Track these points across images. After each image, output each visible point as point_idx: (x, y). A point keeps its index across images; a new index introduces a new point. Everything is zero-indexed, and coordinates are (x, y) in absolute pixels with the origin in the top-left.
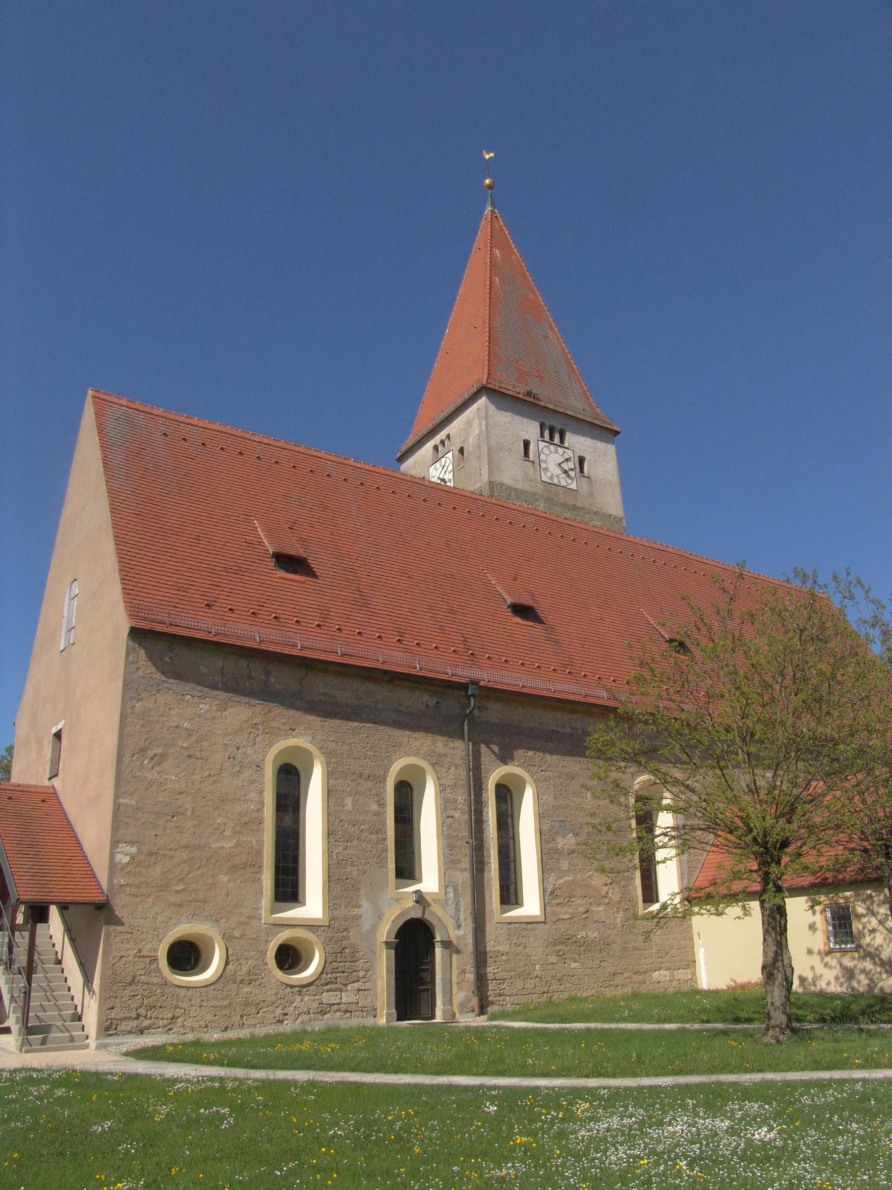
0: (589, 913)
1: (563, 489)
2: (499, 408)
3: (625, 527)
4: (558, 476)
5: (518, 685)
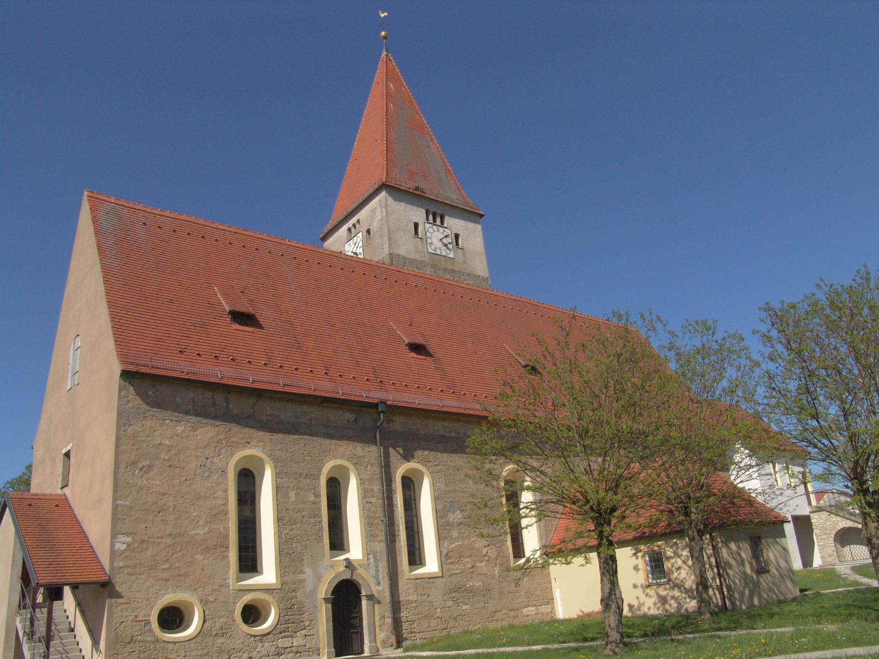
2: (395, 199)
4: (440, 248)
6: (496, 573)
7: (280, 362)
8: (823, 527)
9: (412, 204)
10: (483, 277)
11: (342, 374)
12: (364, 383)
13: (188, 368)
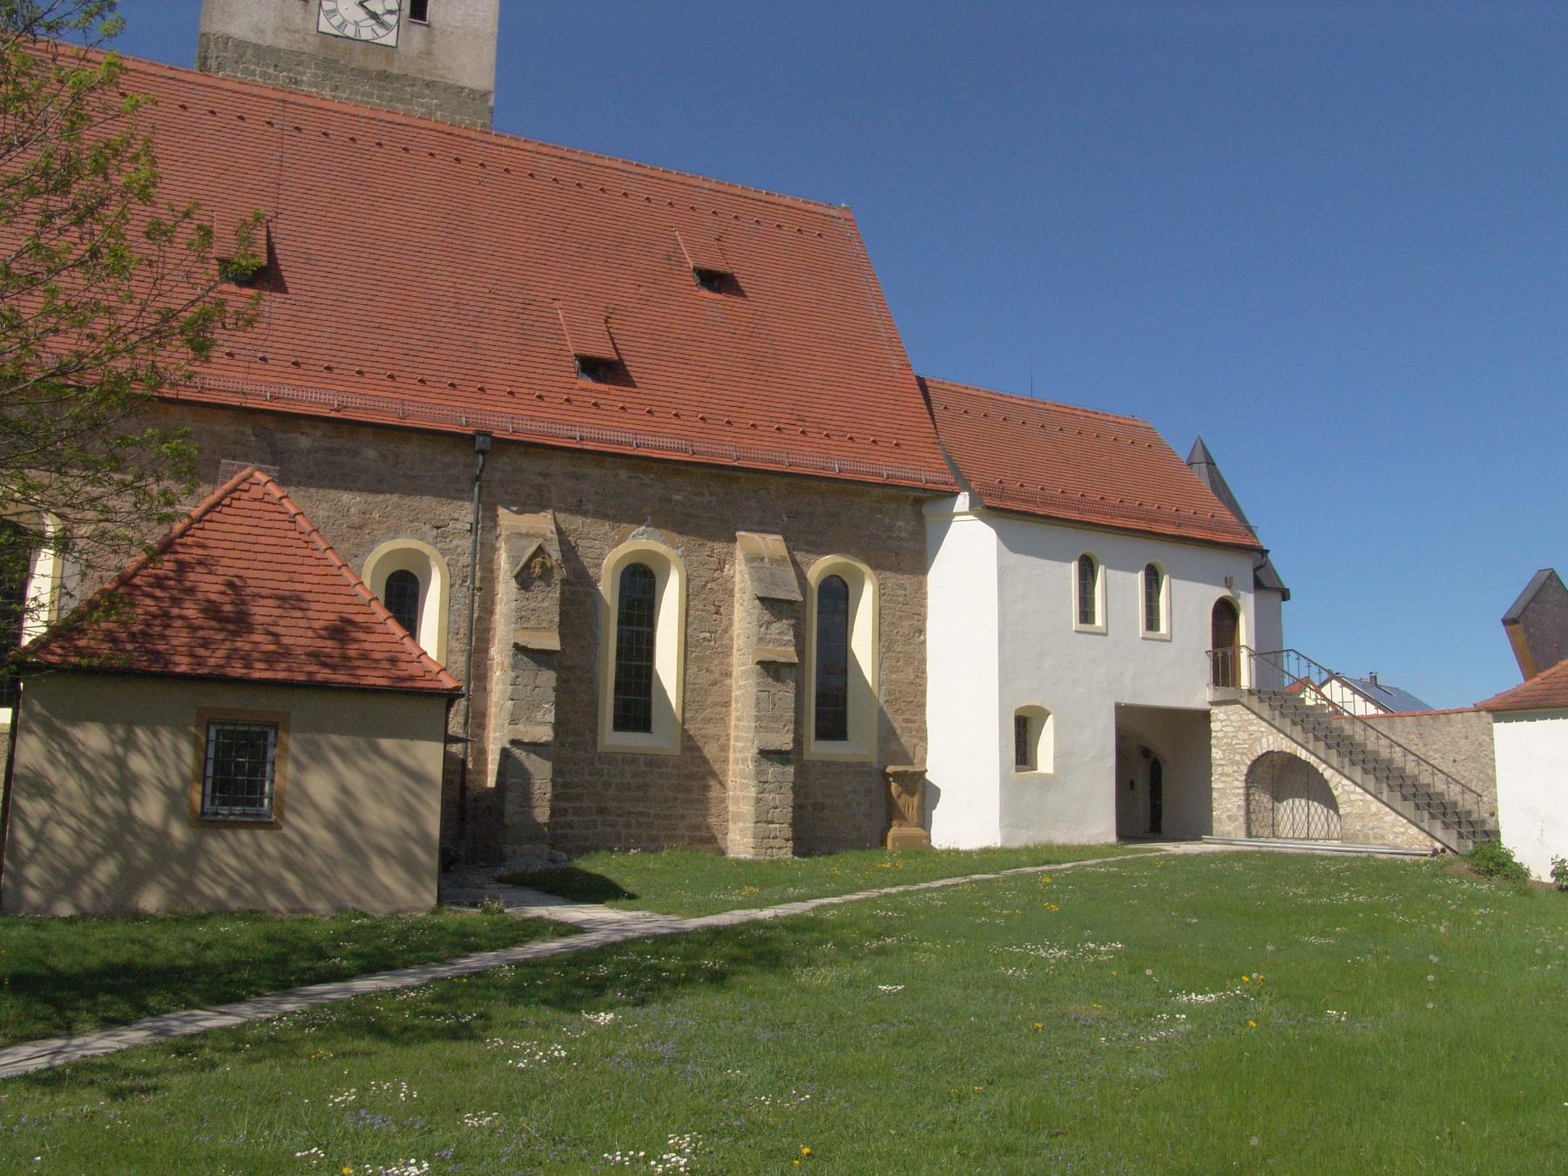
1: (364, 45)
4: (357, 23)
5: (881, 475)
7: (752, 417)
8: (1230, 745)
10: (472, 91)
11: (878, 438)
12: (867, 447)
13: (340, 399)
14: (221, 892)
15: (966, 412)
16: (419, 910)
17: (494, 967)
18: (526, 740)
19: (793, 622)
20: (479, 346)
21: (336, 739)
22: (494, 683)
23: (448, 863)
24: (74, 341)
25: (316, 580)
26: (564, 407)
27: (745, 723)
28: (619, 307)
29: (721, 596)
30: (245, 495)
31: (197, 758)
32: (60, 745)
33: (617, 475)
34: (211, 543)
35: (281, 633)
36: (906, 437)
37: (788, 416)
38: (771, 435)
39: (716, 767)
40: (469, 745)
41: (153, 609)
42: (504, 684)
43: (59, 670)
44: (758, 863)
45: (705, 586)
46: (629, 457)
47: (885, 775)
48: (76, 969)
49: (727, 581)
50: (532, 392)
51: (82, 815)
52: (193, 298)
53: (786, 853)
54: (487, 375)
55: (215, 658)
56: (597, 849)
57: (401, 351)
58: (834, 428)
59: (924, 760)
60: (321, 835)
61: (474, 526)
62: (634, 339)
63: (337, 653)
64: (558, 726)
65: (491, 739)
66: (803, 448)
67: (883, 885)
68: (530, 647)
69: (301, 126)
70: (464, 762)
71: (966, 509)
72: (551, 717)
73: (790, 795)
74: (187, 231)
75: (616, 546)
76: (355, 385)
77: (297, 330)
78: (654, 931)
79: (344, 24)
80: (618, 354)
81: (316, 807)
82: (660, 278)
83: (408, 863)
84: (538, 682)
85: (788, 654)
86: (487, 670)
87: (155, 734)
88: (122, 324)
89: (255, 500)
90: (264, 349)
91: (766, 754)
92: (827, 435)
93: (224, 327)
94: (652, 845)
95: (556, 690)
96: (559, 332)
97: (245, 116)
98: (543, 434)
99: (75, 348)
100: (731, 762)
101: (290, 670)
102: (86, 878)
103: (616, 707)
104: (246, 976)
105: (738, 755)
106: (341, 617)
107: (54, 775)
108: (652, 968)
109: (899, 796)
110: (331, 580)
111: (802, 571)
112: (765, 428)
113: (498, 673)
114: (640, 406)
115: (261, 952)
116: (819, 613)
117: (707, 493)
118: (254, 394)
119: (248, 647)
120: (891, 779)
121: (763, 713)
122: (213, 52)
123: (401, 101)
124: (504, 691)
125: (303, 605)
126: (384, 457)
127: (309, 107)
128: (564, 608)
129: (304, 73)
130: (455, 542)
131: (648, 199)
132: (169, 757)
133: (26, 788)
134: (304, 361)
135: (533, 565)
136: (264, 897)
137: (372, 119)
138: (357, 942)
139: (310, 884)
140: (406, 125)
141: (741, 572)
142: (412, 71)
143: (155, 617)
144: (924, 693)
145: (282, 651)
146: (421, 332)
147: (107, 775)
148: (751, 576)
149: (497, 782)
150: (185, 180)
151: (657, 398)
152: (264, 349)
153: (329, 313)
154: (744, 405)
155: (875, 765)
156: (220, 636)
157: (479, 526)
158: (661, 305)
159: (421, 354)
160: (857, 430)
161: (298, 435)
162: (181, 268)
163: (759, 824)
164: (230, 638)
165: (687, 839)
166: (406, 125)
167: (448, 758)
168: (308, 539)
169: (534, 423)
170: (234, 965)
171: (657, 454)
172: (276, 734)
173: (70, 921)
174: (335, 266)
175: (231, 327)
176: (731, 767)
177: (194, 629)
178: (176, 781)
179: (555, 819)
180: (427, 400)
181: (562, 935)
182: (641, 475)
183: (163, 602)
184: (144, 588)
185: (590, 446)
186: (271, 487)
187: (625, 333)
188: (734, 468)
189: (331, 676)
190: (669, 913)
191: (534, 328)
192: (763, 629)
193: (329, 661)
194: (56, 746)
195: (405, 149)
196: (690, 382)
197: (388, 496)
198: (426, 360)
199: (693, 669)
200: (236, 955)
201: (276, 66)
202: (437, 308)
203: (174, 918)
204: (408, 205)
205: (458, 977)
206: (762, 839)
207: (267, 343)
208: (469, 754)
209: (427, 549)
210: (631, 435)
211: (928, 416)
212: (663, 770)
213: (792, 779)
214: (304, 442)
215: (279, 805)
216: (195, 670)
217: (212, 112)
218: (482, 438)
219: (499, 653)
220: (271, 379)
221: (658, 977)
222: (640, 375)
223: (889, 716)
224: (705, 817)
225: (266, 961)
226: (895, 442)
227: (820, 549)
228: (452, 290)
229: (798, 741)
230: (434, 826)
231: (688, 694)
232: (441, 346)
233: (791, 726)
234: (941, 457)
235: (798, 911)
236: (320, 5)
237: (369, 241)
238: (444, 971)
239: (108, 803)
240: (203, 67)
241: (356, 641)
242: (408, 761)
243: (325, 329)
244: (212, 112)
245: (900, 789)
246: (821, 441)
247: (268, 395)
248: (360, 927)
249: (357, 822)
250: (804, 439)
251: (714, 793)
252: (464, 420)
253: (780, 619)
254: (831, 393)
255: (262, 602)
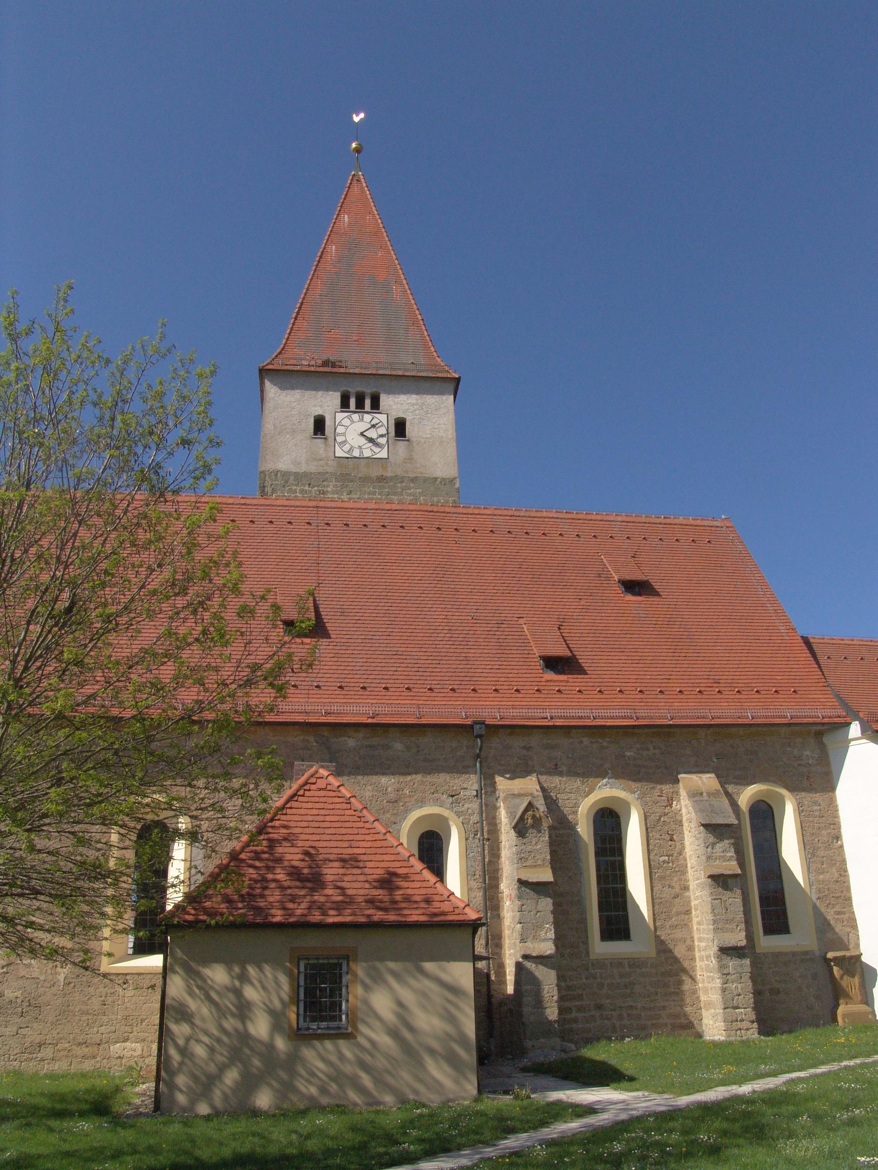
0: (11, 967)
1: (366, 461)
2: (283, 388)
3: (458, 489)
4: (360, 447)
5: (785, 717)
6: (61, 978)
9: (316, 389)
10: (444, 479)
13: (326, 708)
14: (313, 1090)
15: (845, 658)
16: (464, 1099)
17: (528, 1147)
18: (534, 954)
19: (732, 841)
20: (469, 659)
21: (392, 965)
22: (505, 910)
23: (483, 1058)
24: (196, 694)
25: (369, 844)
26: (536, 696)
27: (705, 927)
28: (567, 617)
29: (673, 827)
30: (313, 787)
31: (291, 985)
32: (195, 981)
33: (581, 742)
34: (291, 824)
35: (345, 887)
36: (801, 685)
37: (706, 681)
38: (695, 696)
39: (686, 964)
40: (491, 962)
41: (255, 876)
42: (513, 911)
43: (191, 925)
44: (731, 1043)
45: (660, 819)
46: (590, 727)
47: (827, 961)
48: (215, 1159)
49: (676, 814)
50: (511, 687)
51: (213, 1034)
52: (271, 653)
53: (753, 1034)
54: (478, 679)
55: (300, 910)
56: (598, 1039)
57: (414, 669)
58: (743, 685)
59: (857, 945)
60: (385, 1040)
61: (479, 792)
62: (581, 639)
63: (386, 899)
64: (558, 941)
65: (507, 955)
66: (721, 704)
67: (841, 1058)
68: (530, 880)
69: (330, 522)
70: (488, 976)
71: (859, 734)
72: (551, 935)
73: (750, 983)
74: (263, 608)
75: (587, 796)
76: (383, 697)
77: (339, 664)
78: (653, 1109)
79: (352, 449)
80: (571, 651)
81: (379, 1018)
82: (595, 591)
83: (452, 1059)
84: (539, 908)
85: (732, 867)
86: (499, 901)
87: (261, 969)
88: (226, 677)
89: (320, 789)
90: (318, 679)
91: (726, 951)
92: (738, 692)
93: (293, 672)
94: (641, 1033)
95: (553, 912)
96: (525, 641)
97: (292, 521)
98: (523, 718)
99: (196, 698)
100: (697, 959)
101: (353, 914)
102: (218, 1083)
103: (601, 923)
104: (338, 1161)
105: (703, 953)
106: (387, 871)
107: (193, 1005)
108: (657, 1143)
109: (842, 978)
110: (378, 844)
111: (734, 799)
112: (689, 693)
113: (508, 903)
114: (592, 688)
115: (348, 1140)
116: (752, 831)
117: (652, 748)
118: (315, 713)
119: (322, 899)
120: (832, 964)
121: (718, 917)
122: (268, 483)
123: (395, 494)
124: (513, 918)
125: (361, 864)
126: (408, 748)
127: (334, 508)
128: (553, 848)
129: (328, 486)
130: (466, 806)
131: (578, 535)
132: (271, 985)
133: (174, 1015)
134: (346, 684)
135: (526, 817)
136: (344, 1092)
137: (377, 509)
138: (419, 1129)
139: (378, 1081)
140: (400, 510)
141: (686, 806)
142: (399, 472)
143: (256, 881)
144: (848, 889)
145: (348, 900)
146: (426, 654)
147: (229, 1002)
148: (694, 808)
149: (515, 990)
150: (256, 569)
151: (604, 680)
152: (318, 679)
153: (361, 648)
154: (671, 677)
155: (817, 953)
156: (303, 892)
157: (483, 792)
158: (599, 611)
159: (428, 670)
160: (761, 685)
161: (346, 738)
162: (262, 634)
163: (728, 1010)
164: (310, 893)
165: (669, 1027)
166: (400, 510)
167: (477, 972)
168: (360, 815)
169: (515, 710)
170: (329, 1153)
171: (610, 723)
172: (348, 964)
173: (208, 1118)
174: (361, 614)
175: (298, 670)
176: (698, 963)
177: (283, 888)
178: (277, 1004)
179: (563, 1016)
180: (436, 703)
181: (579, 1116)
182: (599, 740)
183: (260, 870)
184: (247, 861)
185: (559, 723)
186: (331, 779)
187: (574, 635)
188: (670, 726)
189: (386, 917)
190: (663, 1092)
191: (507, 641)
192: (709, 849)
193: (382, 905)
194: (192, 982)
195: (401, 527)
196: (627, 665)
197: (414, 776)
198: (432, 674)
199: (658, 887)
200: (330, 1144)
201: (309, 484)
202: (436, 635)
203: (281, 1114)
204: (408, 565)
205: (500, 1157)
206: (731, 1022)
207: (320, 675)
208: (492, 968)
209: (446, 813)
210: (588, 711)
211: (816, 666)
212: (644, 970)
213: (749, 970)
214: (351, 743)
215: (353, 1020)
216: (287, 919)
217: (271, 522)
218: (478, 726)
219: (507, 887)
220: (324, 700)
221: (663, 1152)
222: (590, 665)
223: (823, 911)
224: (681, 1006)
225: (353, 1148)
226: (793, 690)
227: (746, 780)
228: (445, 621)
229: (750, 937)
230: (470, 1028)
231: (657, 907)
232: (441, 662)
233: (743, 926)
234: (831, 696)
235: (772, 1086)
236: (335, 439)
237: (383, 594)
238: (489, 1152)
239: (230, 1023)
240: (263, 493)
241: (399, 888)
242: (444, 977)
243: (359, 660)
244: (271, 522)
245: (842, 972)
246: (734, 697)
247: (323, 711)
248: (421, 1116)
249: (411, 1029)
250: (720, 696)
251: (687, 986)
252: (464, 714)
253: (721, 840)
254: (736, 659)
255: (331, 864)
